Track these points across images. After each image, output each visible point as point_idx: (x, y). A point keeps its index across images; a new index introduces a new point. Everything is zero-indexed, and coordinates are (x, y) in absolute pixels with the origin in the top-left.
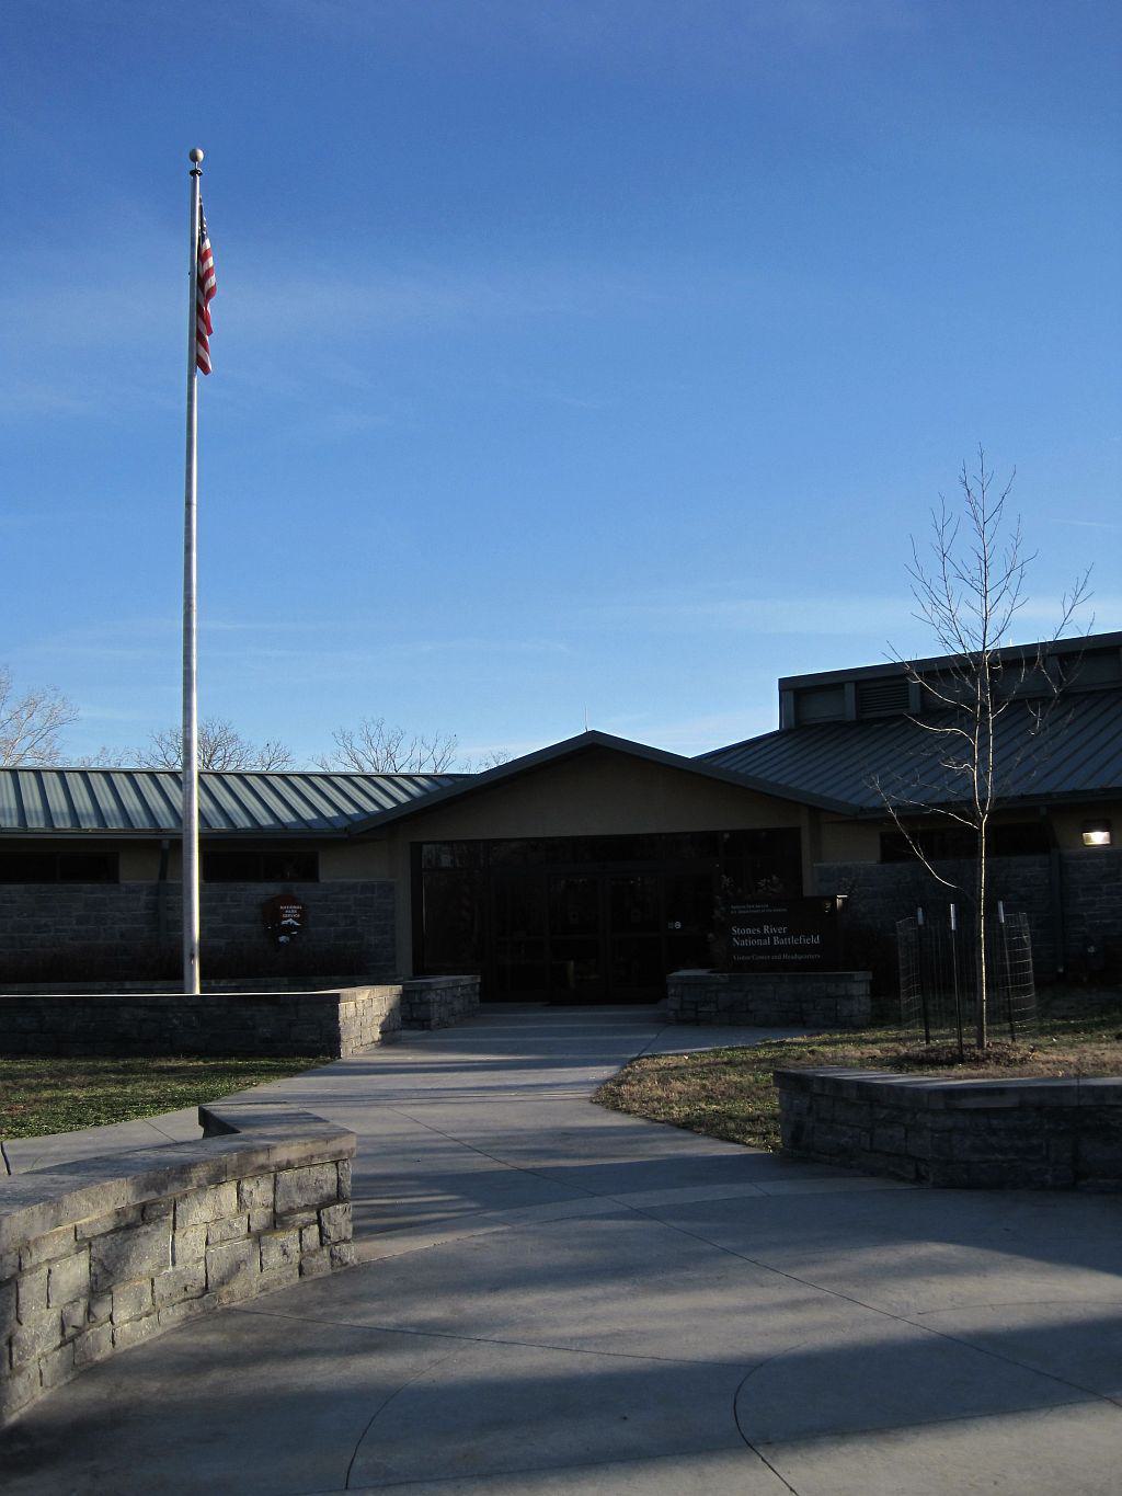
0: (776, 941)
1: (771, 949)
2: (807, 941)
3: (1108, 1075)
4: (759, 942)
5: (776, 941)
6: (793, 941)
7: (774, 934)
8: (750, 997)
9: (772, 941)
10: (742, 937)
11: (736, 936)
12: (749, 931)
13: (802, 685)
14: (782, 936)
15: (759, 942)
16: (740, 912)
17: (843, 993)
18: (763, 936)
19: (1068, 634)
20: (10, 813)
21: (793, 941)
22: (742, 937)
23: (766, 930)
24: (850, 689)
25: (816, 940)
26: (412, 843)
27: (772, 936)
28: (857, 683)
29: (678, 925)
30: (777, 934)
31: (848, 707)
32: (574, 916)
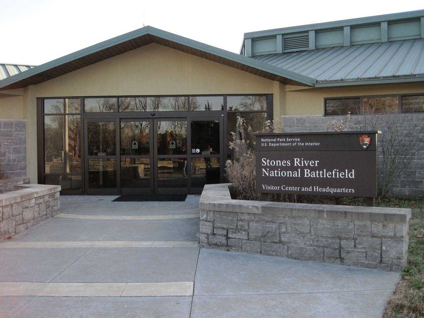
0: (307, 173)
1: (302, 181)
2: (340, 175)
3: (22, 188)
4: (289, 174)
5: (307, 173)
6: (326, 174)
7: (305, 167)
8: (283, 230)
9: (303, 173)
10: (272, 168)
11: (266, 167)
12: (278, 163)
13: (256, 36)
14: (313, 169)
15: (289, 174)
16: (270, 144)
17: (392, 234)
18: (293, 168)
19: (390, 19)
20: (222, 316)
21: (326, 174)
22: (272, 168)
23: (297, 162)
24: (279, 39)
25: (352, 175)
26: (37, 98)
27: (302, 169)
28: (283, 35)
29: (182, 161)
30: (309, 167)
31: (278, 46)
32: (135, 144)
